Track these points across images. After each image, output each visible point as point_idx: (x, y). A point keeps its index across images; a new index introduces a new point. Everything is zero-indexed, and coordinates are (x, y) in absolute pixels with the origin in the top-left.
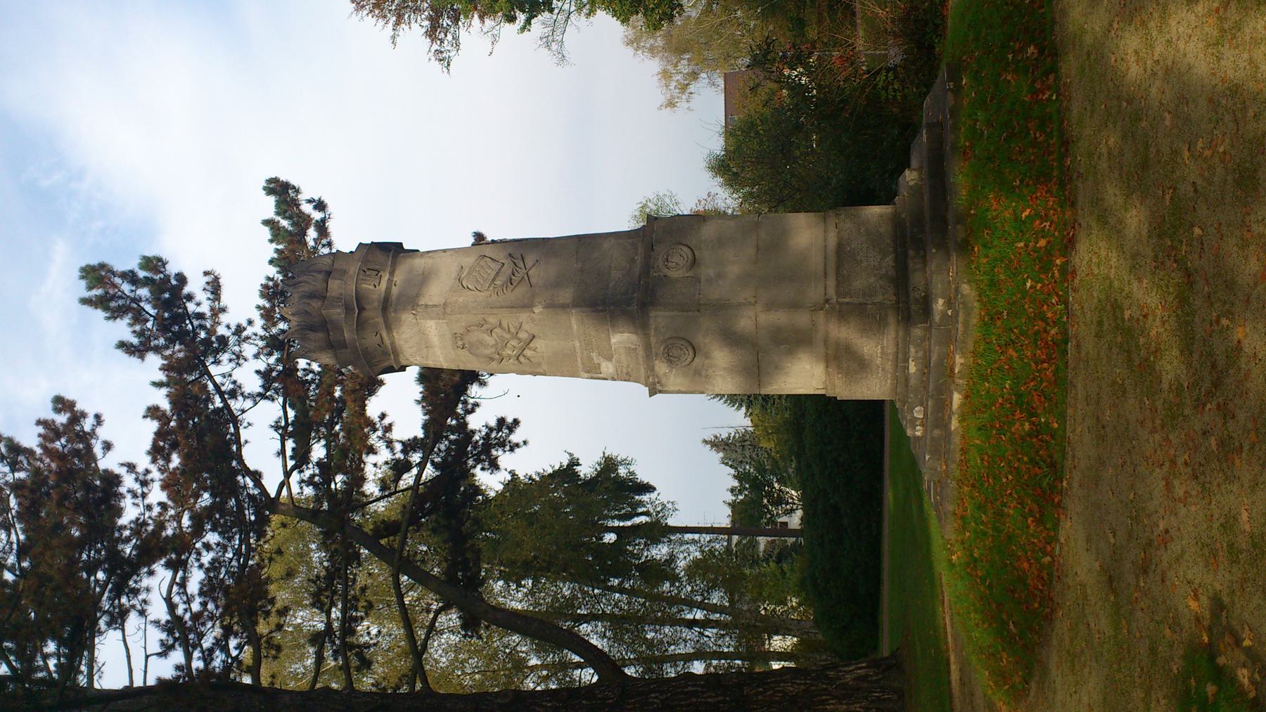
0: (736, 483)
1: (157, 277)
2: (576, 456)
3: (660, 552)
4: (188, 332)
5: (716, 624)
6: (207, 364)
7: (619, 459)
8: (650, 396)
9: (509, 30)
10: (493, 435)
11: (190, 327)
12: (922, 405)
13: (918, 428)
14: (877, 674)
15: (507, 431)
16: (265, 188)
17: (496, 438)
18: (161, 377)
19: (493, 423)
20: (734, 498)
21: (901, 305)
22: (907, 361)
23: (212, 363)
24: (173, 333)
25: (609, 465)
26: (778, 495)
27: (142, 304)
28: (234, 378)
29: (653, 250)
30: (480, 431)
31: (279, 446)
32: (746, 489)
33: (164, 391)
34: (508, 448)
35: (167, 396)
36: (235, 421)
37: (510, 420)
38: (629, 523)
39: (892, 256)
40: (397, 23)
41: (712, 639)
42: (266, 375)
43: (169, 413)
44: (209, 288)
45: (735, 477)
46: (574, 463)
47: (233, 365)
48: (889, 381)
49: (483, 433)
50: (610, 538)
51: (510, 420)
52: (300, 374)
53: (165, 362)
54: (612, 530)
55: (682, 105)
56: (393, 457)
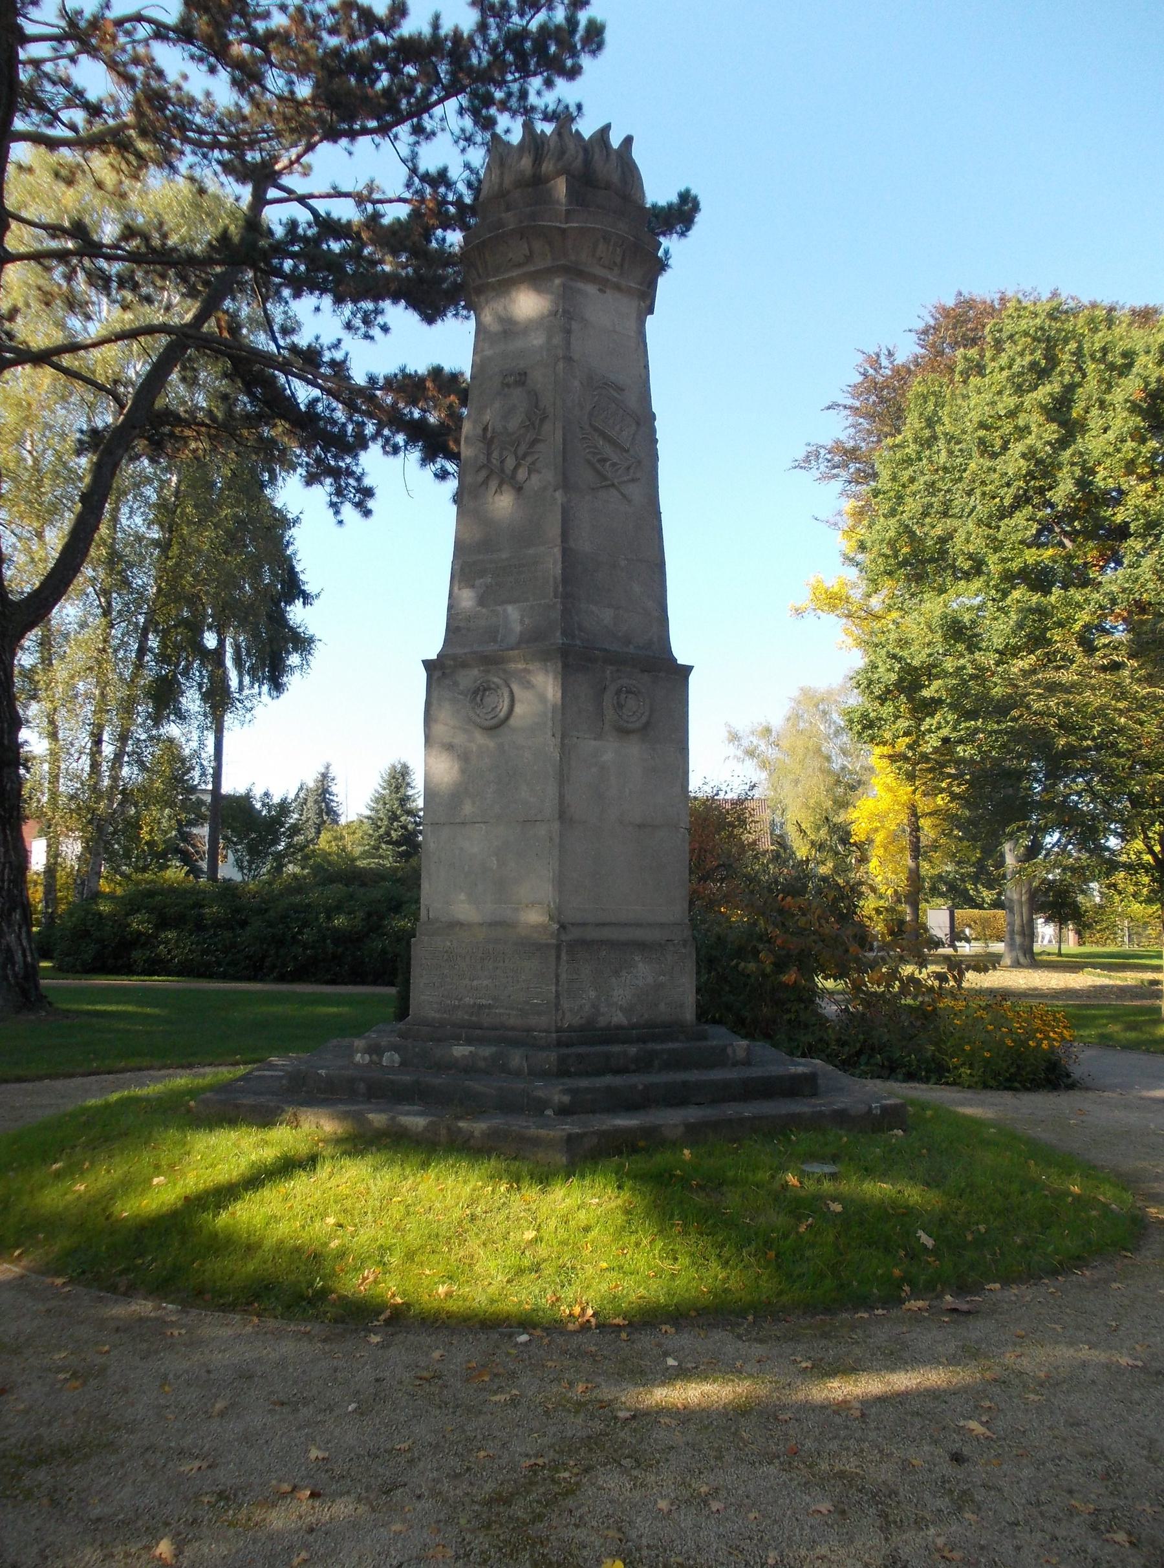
0: (276, 800)
1: (577, 37)
2: (316, 602)
3: (192, 701)
4: (503, 74)
5: (95, 766)
6: (459, 97)
7: (309, 657)
8: (424, 662)
9: (841, 543)
10: (352, 481)
11: (510, 77)
12: (402, 1064)
13: (367, 1057)
14: (15, 976)
15: (357, 499)
16: (688, 191)
17: (348, 484)
18: (446, 29)
19: (367, 482)
20: (258, 797)
21: (554, 1035)
22: (469, 1041)
23: (461, 104)
24: (503, 53)
25: (302, 643)
26: (261, 852)
27: (544, 10)
28: (440, 134)
29: (643, 671)
30: (357, 465)
31: (345, 188)
32: (269, 812)
33: (427, 31)
34: (335, 499)
35: (420, 34)
36: (384, 130)
37: (371, 504)
38: (229, 663)
39: (625, 1022)
40: (855, 410)
41: (75, 764)
42: (441, 178)
43: (396, 34)
44: (561, 108)
45: (284, 801)
46: (307, 598)
47: (457, 132)
48: (437, 1016)
49: (354, 468)
50: (210, 640)
51: (371, 504)
52: (439, 232)
53: (465, 35)
54: (221, 642)
55: (731, 750)
56: (325, 348)
